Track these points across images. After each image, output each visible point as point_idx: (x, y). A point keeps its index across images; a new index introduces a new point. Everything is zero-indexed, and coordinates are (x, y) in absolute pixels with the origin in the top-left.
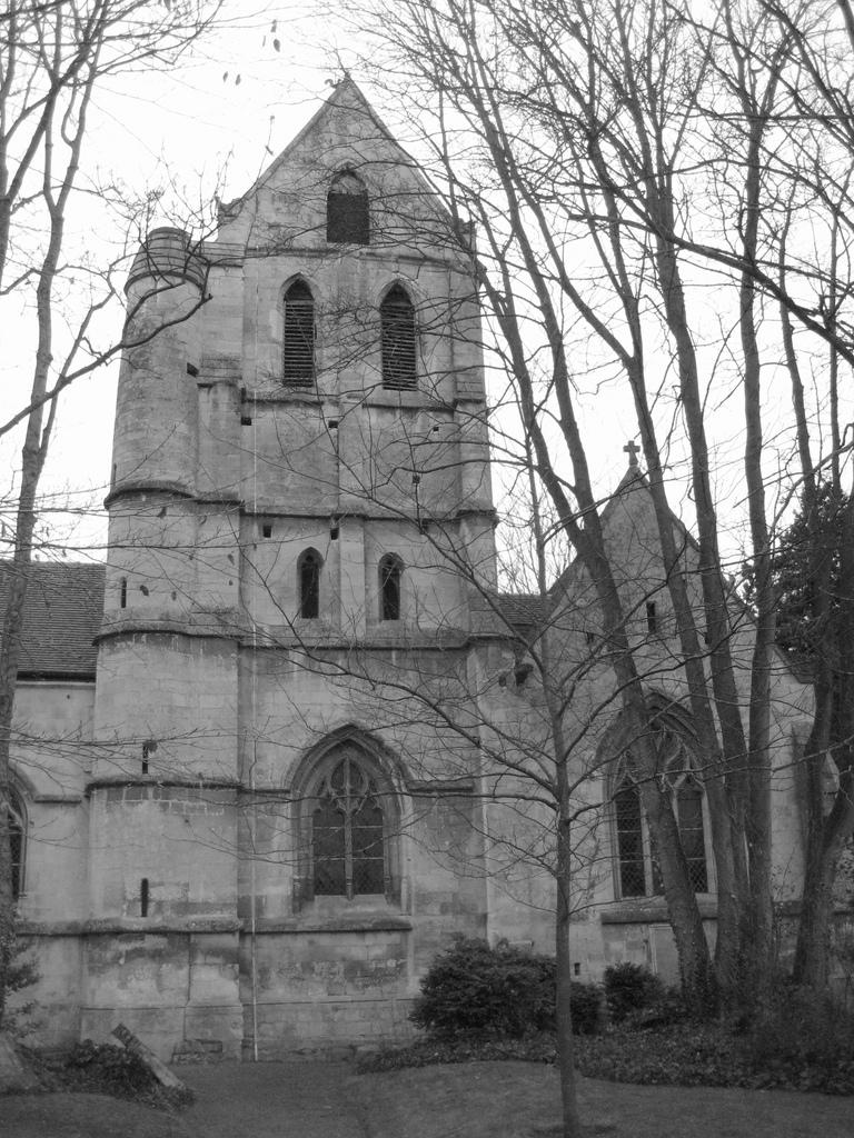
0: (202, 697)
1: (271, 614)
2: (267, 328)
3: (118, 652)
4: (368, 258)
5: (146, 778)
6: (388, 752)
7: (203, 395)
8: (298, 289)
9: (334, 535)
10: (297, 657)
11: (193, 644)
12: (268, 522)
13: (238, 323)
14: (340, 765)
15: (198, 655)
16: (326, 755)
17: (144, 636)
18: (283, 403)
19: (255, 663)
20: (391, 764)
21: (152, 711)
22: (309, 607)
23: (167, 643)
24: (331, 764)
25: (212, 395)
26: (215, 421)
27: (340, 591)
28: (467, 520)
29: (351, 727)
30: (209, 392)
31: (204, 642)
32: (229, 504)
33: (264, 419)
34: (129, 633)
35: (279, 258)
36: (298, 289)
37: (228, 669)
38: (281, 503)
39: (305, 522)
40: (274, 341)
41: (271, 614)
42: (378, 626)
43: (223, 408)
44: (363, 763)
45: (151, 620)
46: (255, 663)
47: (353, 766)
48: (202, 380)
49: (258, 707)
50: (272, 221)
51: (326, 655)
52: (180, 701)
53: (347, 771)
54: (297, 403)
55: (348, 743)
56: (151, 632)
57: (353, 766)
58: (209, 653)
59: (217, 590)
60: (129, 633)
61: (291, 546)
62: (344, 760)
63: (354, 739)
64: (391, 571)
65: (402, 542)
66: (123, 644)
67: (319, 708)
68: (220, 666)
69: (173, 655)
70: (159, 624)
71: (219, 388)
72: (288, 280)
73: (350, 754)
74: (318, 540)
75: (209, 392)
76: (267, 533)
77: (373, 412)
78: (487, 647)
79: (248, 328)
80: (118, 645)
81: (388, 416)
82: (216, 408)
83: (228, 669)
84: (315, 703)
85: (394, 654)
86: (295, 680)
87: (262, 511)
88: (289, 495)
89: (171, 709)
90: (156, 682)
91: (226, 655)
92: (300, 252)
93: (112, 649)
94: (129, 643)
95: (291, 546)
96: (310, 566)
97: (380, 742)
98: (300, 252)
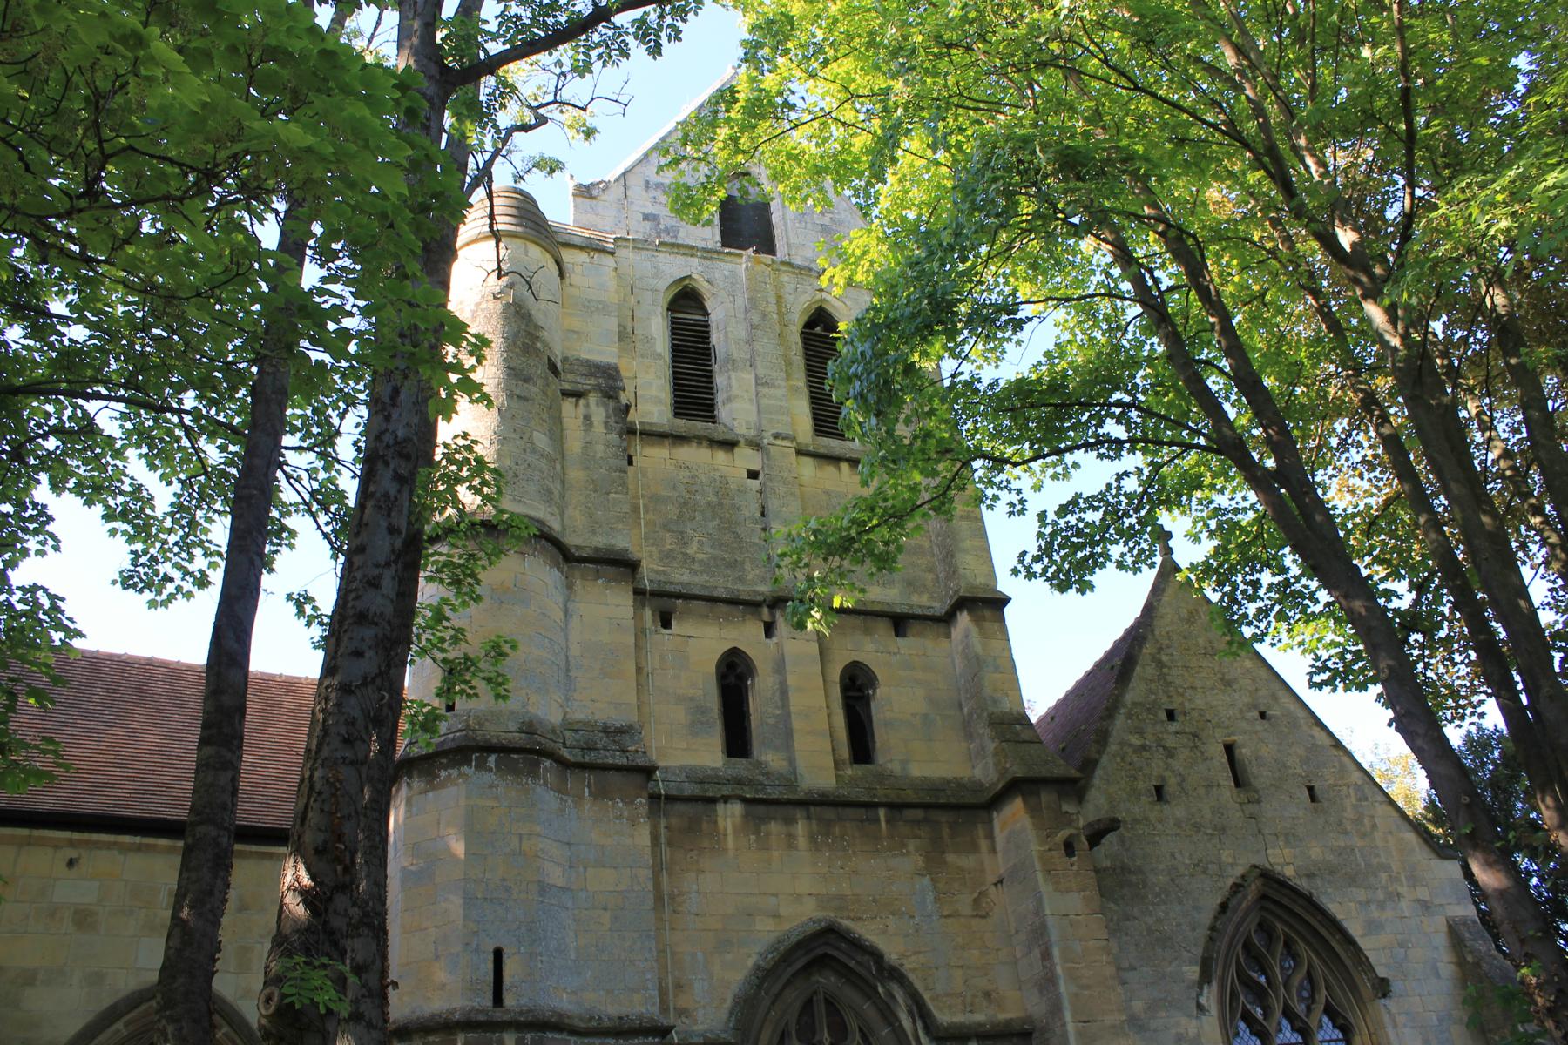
0: (590, 871)
1: (687, 748)
2: (649, 340)
3: (442, 786)
4: (783, 268)
5: (498, 1015)
6: (895, 974)
7: (568, 406)
8: (686, 300)
9: (769, 630)
10: (730, 816)
11: (572, 780)
12: (664, 605)
13: (612, 324)
14: (808, 1004)
15: (581, 797)
16: (788, 983)
17: (492, 759)
18: (678, 439)
19: (663, 823)
20: (899, 994)
21: (508, 889)
22: (737, 741)
23: (533, 770)
24: (794, 999)
25: (581, 410)
26: (588, 445)
27: (789, 715)
28: (970, 612)
29: (831, 932)
30: (577, 405)
31: (591, 777)
32: (621, 565)
33: (653, 458)
34: (466, 751)
35: (661, 256)
36: (686, 300)
37: (633, 822)
38: (681, 577)
39: (724, 608)
40: (659, 356)
41: (687, 748)
42: (849, 772)
43: (599, 428)
44: (849, 995)
45: (508, 731)
46: (663, 823)
47: (829, 1003)
48: (567, 386)
49: (672, 897)
50: (647, 211)
51: (773, 804)
52: (556, 876)
53: (820, 1009)
54: (699, 439)
55: (822, 962)
56: (503, 750)
57: (829, 1003)
58: (601, 794)
59: (600, 699)
60: (466, 751)
61: (703, 642)
62: (815, 993)
63: (835, 953)
64: (856, 687)
65: (870, 647)
66: (454, 772)
67: (773, 900)
68: (620, 817)
69: (544, 794)
70: (518, 739)
71: (593, 399)
72: (671, 285)
73: (826, 980)
74: (746, 635)
75: (577, 405)
76: (666, 624)
77: (808, 461)
78: (1039, 795)
79: (625, 336)
80: (443, 774)
81: (830, 469)
82: (584, 424)
83: (633, 822)
84: (768, 889)
85: (882, 813)
86: (731, 853)
87: (655, 587)
88: (696, 566)
89: (544, 888)
90: (515, 841)
91: (629, 802)
92: (690, 250)
93: (430, 782)
94: (465, 769)
95: (703, 642)
96: (734, 674)
97: (876, 955)
98: (690, 250)
